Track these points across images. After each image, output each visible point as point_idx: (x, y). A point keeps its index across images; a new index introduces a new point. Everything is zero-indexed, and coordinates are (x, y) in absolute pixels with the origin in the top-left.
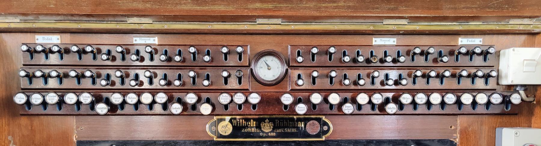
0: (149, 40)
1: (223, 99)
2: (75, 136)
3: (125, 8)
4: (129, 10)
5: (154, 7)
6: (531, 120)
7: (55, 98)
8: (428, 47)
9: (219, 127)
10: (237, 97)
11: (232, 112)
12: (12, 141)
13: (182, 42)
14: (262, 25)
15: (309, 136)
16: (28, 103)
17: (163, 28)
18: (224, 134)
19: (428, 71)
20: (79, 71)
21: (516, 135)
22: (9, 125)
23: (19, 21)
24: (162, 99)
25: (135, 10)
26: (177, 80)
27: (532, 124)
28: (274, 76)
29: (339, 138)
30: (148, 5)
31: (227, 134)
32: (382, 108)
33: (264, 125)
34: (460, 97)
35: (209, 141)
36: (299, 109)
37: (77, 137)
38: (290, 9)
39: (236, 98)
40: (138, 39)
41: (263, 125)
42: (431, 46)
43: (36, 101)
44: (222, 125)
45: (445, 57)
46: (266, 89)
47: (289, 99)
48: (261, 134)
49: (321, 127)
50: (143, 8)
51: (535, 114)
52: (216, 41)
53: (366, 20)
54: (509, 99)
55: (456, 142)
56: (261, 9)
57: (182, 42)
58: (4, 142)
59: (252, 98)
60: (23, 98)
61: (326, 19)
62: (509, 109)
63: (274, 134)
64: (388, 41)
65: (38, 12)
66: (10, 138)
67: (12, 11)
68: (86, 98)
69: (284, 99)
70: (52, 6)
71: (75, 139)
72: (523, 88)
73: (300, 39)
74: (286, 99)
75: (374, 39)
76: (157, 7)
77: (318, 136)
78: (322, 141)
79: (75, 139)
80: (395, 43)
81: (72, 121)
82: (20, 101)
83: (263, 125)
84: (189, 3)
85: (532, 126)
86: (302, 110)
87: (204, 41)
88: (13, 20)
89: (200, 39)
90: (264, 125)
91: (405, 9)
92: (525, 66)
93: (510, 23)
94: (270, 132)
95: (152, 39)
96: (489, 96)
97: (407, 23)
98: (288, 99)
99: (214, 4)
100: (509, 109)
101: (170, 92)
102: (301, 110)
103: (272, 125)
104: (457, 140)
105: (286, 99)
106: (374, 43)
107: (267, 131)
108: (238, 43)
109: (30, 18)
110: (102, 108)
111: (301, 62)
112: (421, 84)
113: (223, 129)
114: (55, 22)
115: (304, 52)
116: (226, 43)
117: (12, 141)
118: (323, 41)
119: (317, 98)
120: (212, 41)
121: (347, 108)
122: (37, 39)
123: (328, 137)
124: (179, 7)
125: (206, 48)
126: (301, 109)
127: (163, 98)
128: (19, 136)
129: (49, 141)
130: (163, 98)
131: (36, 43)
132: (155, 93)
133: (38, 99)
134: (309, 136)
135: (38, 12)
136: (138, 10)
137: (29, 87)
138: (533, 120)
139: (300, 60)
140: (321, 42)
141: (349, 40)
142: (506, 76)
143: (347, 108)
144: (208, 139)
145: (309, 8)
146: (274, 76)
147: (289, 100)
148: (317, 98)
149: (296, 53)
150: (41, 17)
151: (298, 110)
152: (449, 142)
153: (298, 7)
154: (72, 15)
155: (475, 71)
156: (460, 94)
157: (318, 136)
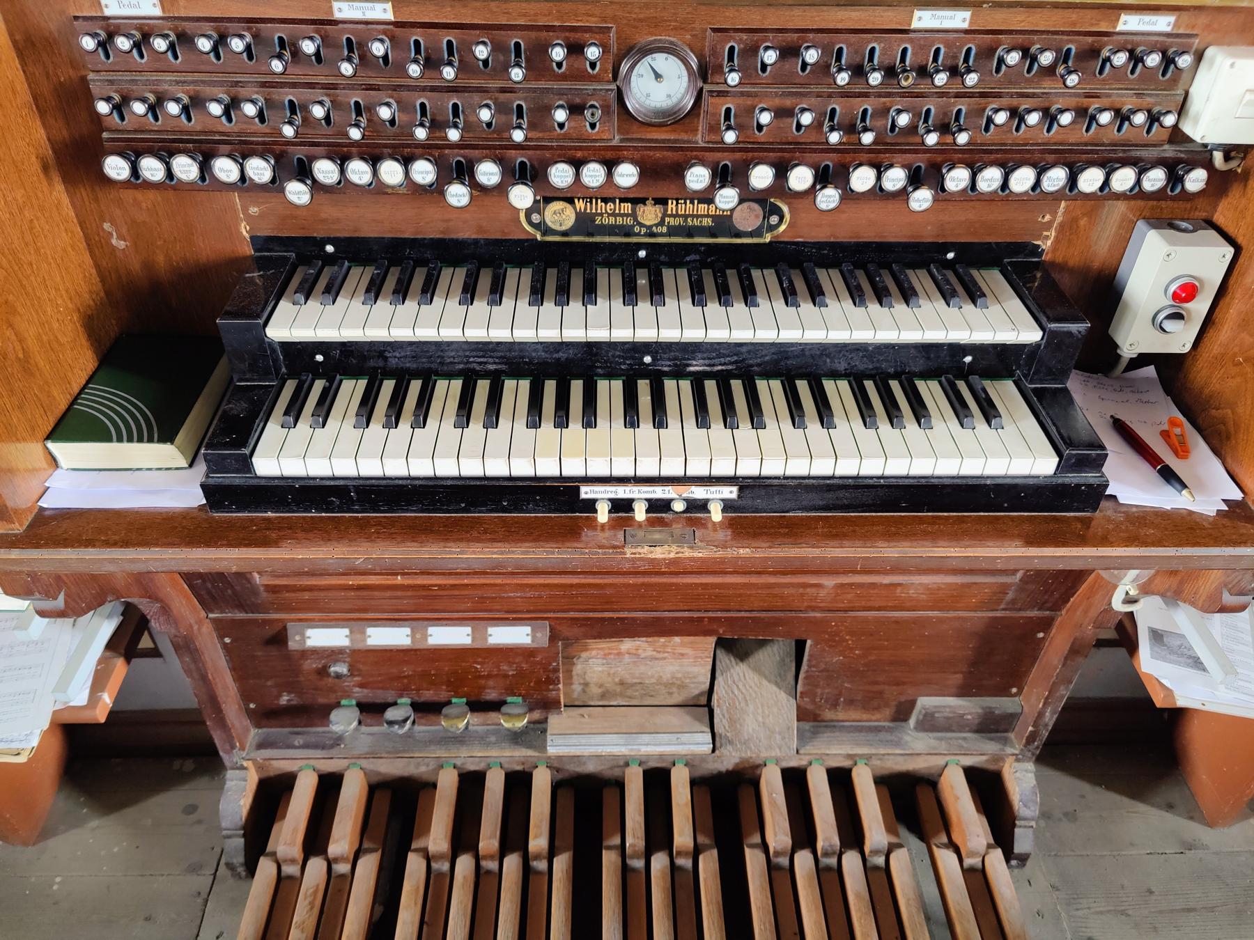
0: (373, 9)
1: (558, 176)
2: (243, 225)
6: (1218, 205)
7: (192, 169)
9: (546, 213)
10: (588, 173)
12: (114, 234)
13: (453, 16)
15: (738, 234)
18: (557, 227)
21: (1166, 258)
22: (96, 200)
24: (425, 175)
27: (1217, 213)
28: (669, 96)
29: (800, 237)
31: (564, 228)
33: (644, 212)
35: (527, 240)
36: (722, 200)
37: (248, 228)
39: (586, 176)
41: (642, 210)
44: (553, 209)
46: (650, 132)
47: (703, 179)
49: (764, 218)
51: (1230, 194)
52: (536, 15)
54: (1183, 176)
55: (1044, 247)
57: (453, 16)
58: (98, 235)
59: (622, 175)
60: (124, 168)
64: (951, 18)
66: (107, 226)
69: (691, 179)
71: (245, 233)
73: (737, 11)
74: (695, 179)
75: (917, 14)
77: (757, 233)
78: (765, 244)
79: (245, 233)
80: (965, 26)
83: (642, 210)
86: (728, 202)
87: (505, 13)
89: (495, 10)
90: (644, 212)
92: (1245, 105)
94: (657, 225)
98: (700, 179)
102: (726, 202)
103: (660, 211)
104: (1049, 243)
105: (695, 179)
106: (915, 24)
107: (648, 223)
108: (587, 21)
110: (299, 193)
111: (735, 86)
113: (556, 218)
115: (745, 47)
116: (558, 20)
117: (114, 234)
118: (794, 16)
119: (762, 178)
120: (525, 16)
121: (824, 199)
123: (777, 236)
125: (512, 37)
126: (727, 200)
127: (427, 173)
128: (126, 223)
129: (193, 234)
130: (427, 173)
133: (155, 170)
134: (738, 234)
139: (733, 80)
140: (788, 18)
141: (857, 14)
143: (824, 199)
144: (523, 237)
146: (669, 96)
147: (701, 181)
148: (762, 178)
149: (724, 52)
151: (720, 202)
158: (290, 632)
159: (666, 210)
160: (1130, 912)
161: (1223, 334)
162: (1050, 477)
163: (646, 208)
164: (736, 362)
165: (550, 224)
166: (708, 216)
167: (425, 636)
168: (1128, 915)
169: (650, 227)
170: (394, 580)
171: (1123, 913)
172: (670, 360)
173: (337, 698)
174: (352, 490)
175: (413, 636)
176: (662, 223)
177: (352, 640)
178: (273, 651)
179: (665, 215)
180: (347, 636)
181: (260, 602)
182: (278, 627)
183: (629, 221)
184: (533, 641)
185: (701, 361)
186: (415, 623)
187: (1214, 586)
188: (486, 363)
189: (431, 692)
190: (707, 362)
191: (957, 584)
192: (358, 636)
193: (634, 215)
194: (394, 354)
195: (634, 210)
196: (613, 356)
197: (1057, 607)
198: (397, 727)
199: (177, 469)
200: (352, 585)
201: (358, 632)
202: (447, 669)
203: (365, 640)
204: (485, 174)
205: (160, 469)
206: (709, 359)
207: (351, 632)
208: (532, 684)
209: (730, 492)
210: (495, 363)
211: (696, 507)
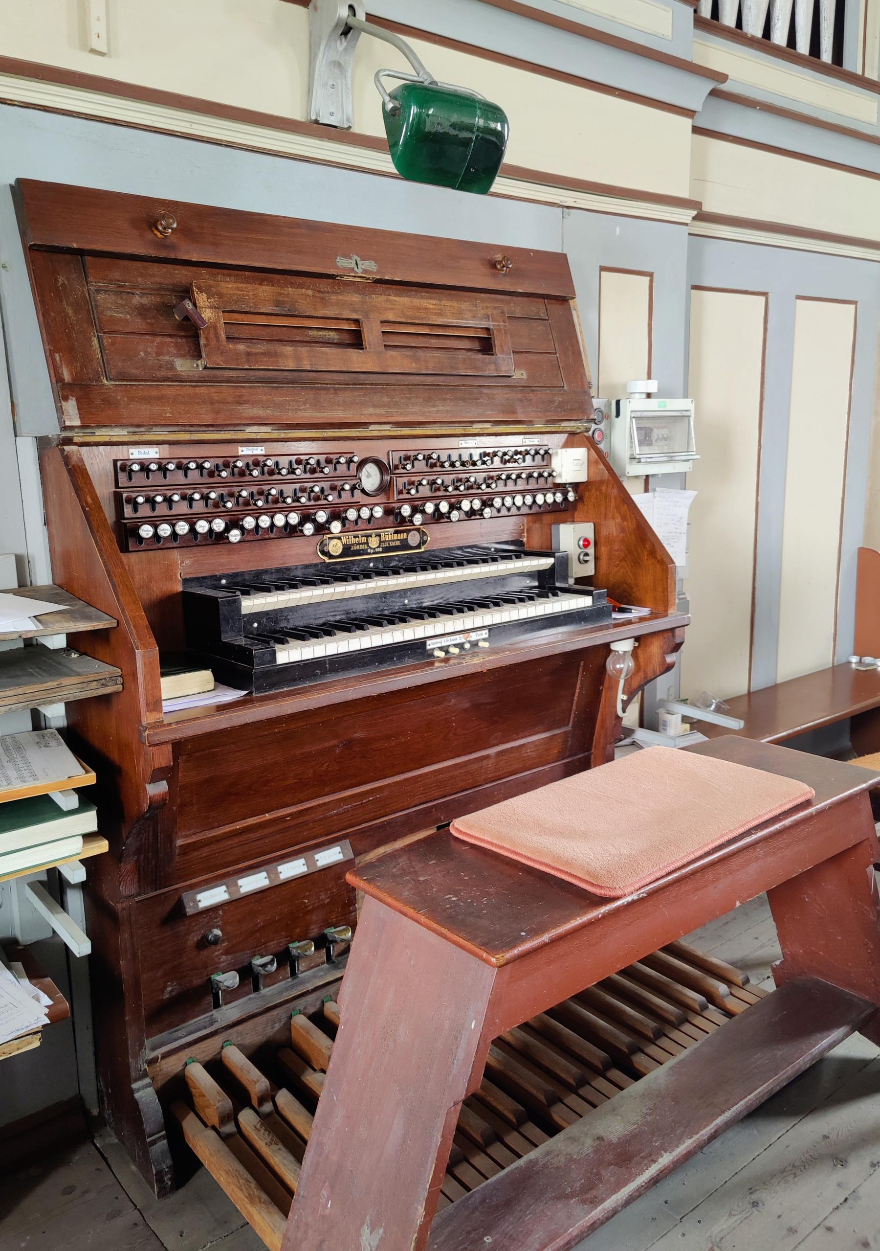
0: (257, 449)
3: (246, 416)
4: (252, 418)
5: (275, 414)
8: (188, 460)
11: (350, 528)
14: (374, 431)
16: (156, 535)
17: (279, 437)
19: (189, 492)
20: (432, 478)
23: (126, 434)
25: (257, 417)
26: (139, 504)
30: (269, 412)
31: (337, 554)
32: (480, 513)
34: (195, 523)
38: (400, 414)
40: (463, 442)
42: (170, 460)
43: (165, 533)
45: (326, 469)
48: (369, 551)
50: (265, 414)
53: (67, 432)
56: (376, 415)
61: (430, 424)
62: (563, 506)
63: (380, 549)
65: (155, 422)
67: (124, 422)
68: (294, 518)
70: (168, 415)
72: (572, 486)
76: (279, 414)
77: (418, 547)
81: (176, 555)
82: (147, 534)
84: (308, 408)
85: (575, 520)
88: (118, 432)
91: (490, 413)
93: (562, 425)
94: (377, 547)
95: (259, 448)
96: (471, 502)
97: (490, 427)
99: (332, 410)
100: (563, 506)
101: (338, 507)
107: (374, 547)
109: (142, 429)
111: (226, 478)
112: (182, 508)
114: (82, 434)
122: (132, 454)
124: (300, 414)
131: (131, 458)
132: (140, 524)
135: (155, 422)
136: (260, 418)
137: (135, 516)
138: (576, 514)
142: (560, 475)
145: (416, 413)
146: (373, 485)
150: (154, 429)
152: (519, 543)
153: (406, 411)
154: (192, 426)
155: (342, 483)
156: (438, 501)
157: (418, 547)
158: (186, 901)
159: (380, 539)
160: (703, 936)
161: (604, 562)
162: (591, 606)
163: (372, 539)
164: (442, 598)
165: (331, 552)
166: (398, 540)
167: (278, 874)
168: (704, 937)
169: (374, 549)
170: (265, 817)
171: (700, 938)
172: (416, 600)
173: (207, 976)
174: (327, 663)
175: (269, 877)
176: (379, 547)
177: (230, 894)
178: (542, 507)
179: (381, 542)
180: (225, 892)
181: (170, 870)
182: (173, 902)
183: (365, 547)
184: (344, 856)
185: (428, 599)
186: (267, 867)
187: (659, 658)
188: (335, 615)
189: (275, 942)
190: (431, 599)
191: (547, 737)
192: (233, 889)
193: (367, 543)
194: (293, 616)
195: (367, 540)
196: (392, 601)
197: (589, 749)
198: (269, 966)
199: (203, 692)
200: (239, 828)
201: (232, 887)
202: (286, 911)
203: (239, 891)
204: (200, 526)
205: (199, 693)
206: (432, 597)
207: (227, 887)
208: (340, 910)
209: (485, 634)
210: (340, 615)
211: (475, 644)
